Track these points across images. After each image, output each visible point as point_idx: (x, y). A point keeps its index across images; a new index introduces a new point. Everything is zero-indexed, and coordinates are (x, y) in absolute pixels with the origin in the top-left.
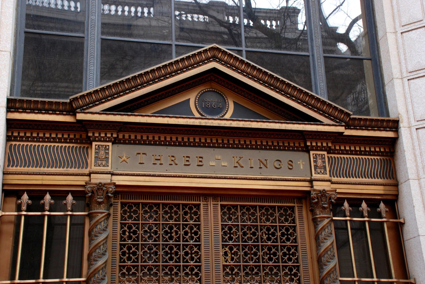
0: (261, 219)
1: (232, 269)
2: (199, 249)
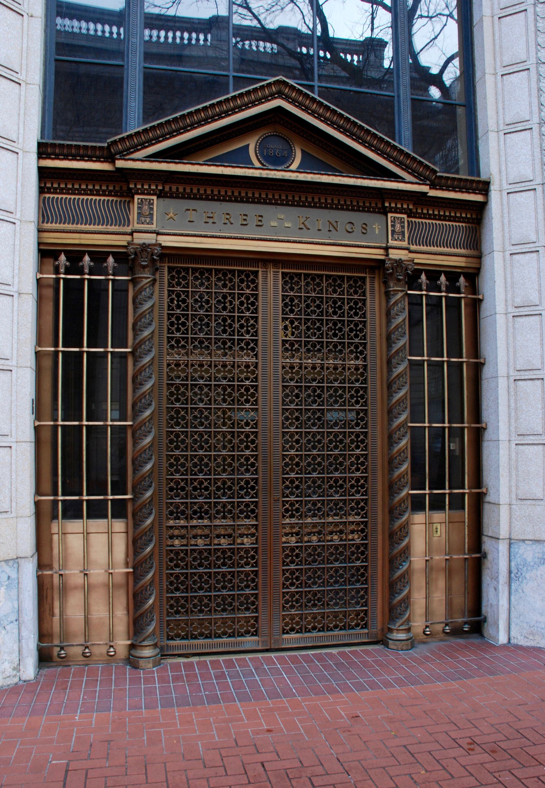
0: (327, 290)
1: (292, 345)
2: (256, 321)
